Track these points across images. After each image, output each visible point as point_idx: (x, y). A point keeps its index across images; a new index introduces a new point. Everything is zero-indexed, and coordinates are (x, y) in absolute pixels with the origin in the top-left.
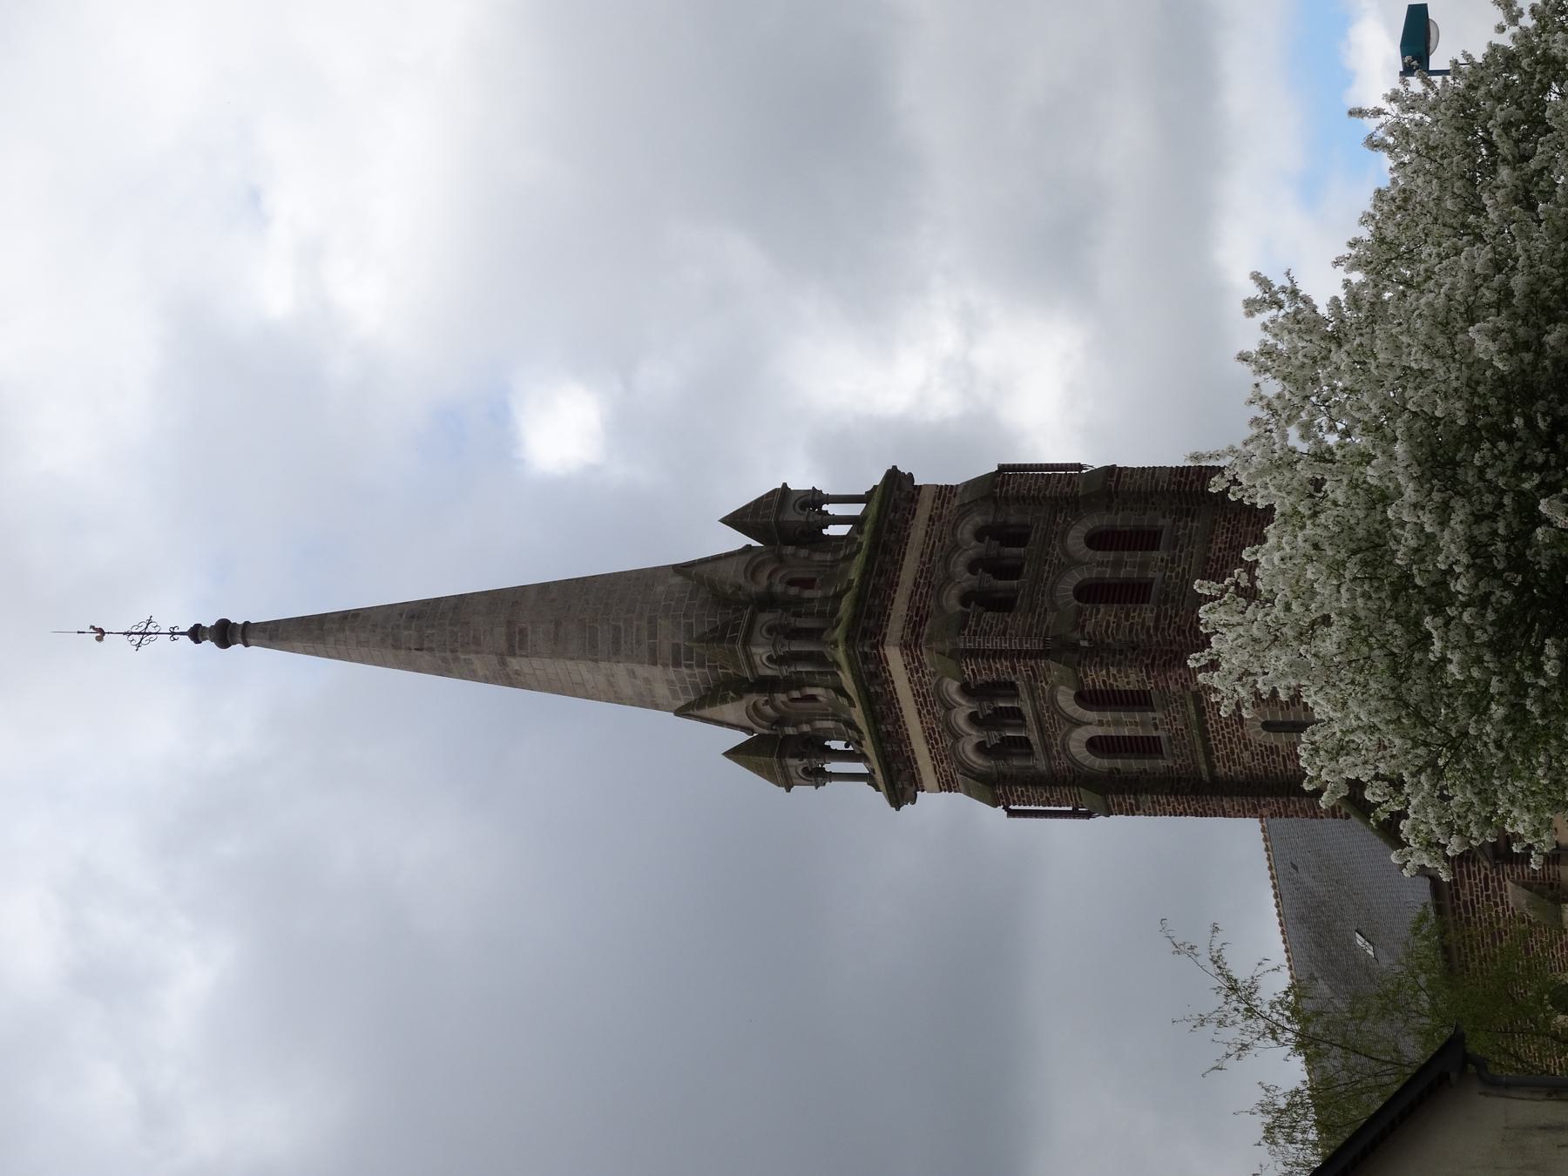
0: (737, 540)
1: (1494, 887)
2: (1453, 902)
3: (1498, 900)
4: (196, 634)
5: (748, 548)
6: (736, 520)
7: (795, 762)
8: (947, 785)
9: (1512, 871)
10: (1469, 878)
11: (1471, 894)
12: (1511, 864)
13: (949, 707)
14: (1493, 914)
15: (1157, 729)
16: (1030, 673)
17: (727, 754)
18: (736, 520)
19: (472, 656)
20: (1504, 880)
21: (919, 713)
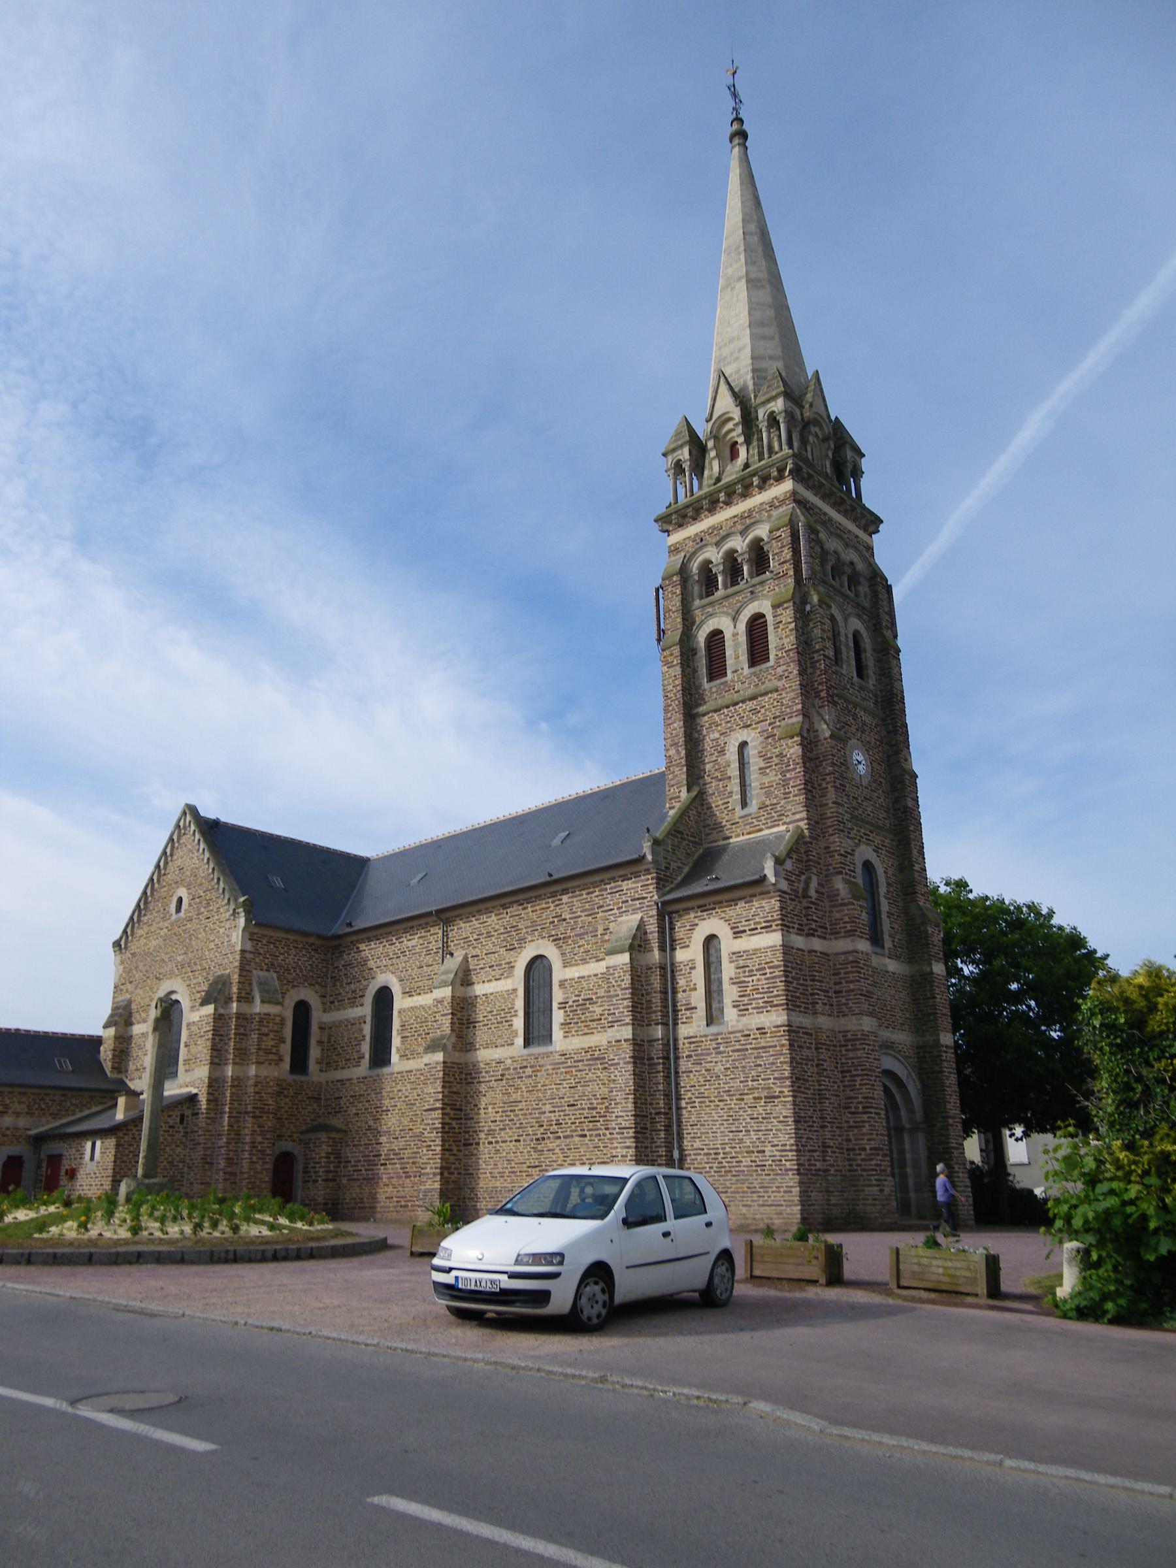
0: (833, 418)
2: (620, 876)
6: (837, 418)
7: (687, 456)
9: (651, 917)
13: (743, 533)
15: (733, 672)
18: (837, 418)
19: (743, 260)
21: (735, 517)
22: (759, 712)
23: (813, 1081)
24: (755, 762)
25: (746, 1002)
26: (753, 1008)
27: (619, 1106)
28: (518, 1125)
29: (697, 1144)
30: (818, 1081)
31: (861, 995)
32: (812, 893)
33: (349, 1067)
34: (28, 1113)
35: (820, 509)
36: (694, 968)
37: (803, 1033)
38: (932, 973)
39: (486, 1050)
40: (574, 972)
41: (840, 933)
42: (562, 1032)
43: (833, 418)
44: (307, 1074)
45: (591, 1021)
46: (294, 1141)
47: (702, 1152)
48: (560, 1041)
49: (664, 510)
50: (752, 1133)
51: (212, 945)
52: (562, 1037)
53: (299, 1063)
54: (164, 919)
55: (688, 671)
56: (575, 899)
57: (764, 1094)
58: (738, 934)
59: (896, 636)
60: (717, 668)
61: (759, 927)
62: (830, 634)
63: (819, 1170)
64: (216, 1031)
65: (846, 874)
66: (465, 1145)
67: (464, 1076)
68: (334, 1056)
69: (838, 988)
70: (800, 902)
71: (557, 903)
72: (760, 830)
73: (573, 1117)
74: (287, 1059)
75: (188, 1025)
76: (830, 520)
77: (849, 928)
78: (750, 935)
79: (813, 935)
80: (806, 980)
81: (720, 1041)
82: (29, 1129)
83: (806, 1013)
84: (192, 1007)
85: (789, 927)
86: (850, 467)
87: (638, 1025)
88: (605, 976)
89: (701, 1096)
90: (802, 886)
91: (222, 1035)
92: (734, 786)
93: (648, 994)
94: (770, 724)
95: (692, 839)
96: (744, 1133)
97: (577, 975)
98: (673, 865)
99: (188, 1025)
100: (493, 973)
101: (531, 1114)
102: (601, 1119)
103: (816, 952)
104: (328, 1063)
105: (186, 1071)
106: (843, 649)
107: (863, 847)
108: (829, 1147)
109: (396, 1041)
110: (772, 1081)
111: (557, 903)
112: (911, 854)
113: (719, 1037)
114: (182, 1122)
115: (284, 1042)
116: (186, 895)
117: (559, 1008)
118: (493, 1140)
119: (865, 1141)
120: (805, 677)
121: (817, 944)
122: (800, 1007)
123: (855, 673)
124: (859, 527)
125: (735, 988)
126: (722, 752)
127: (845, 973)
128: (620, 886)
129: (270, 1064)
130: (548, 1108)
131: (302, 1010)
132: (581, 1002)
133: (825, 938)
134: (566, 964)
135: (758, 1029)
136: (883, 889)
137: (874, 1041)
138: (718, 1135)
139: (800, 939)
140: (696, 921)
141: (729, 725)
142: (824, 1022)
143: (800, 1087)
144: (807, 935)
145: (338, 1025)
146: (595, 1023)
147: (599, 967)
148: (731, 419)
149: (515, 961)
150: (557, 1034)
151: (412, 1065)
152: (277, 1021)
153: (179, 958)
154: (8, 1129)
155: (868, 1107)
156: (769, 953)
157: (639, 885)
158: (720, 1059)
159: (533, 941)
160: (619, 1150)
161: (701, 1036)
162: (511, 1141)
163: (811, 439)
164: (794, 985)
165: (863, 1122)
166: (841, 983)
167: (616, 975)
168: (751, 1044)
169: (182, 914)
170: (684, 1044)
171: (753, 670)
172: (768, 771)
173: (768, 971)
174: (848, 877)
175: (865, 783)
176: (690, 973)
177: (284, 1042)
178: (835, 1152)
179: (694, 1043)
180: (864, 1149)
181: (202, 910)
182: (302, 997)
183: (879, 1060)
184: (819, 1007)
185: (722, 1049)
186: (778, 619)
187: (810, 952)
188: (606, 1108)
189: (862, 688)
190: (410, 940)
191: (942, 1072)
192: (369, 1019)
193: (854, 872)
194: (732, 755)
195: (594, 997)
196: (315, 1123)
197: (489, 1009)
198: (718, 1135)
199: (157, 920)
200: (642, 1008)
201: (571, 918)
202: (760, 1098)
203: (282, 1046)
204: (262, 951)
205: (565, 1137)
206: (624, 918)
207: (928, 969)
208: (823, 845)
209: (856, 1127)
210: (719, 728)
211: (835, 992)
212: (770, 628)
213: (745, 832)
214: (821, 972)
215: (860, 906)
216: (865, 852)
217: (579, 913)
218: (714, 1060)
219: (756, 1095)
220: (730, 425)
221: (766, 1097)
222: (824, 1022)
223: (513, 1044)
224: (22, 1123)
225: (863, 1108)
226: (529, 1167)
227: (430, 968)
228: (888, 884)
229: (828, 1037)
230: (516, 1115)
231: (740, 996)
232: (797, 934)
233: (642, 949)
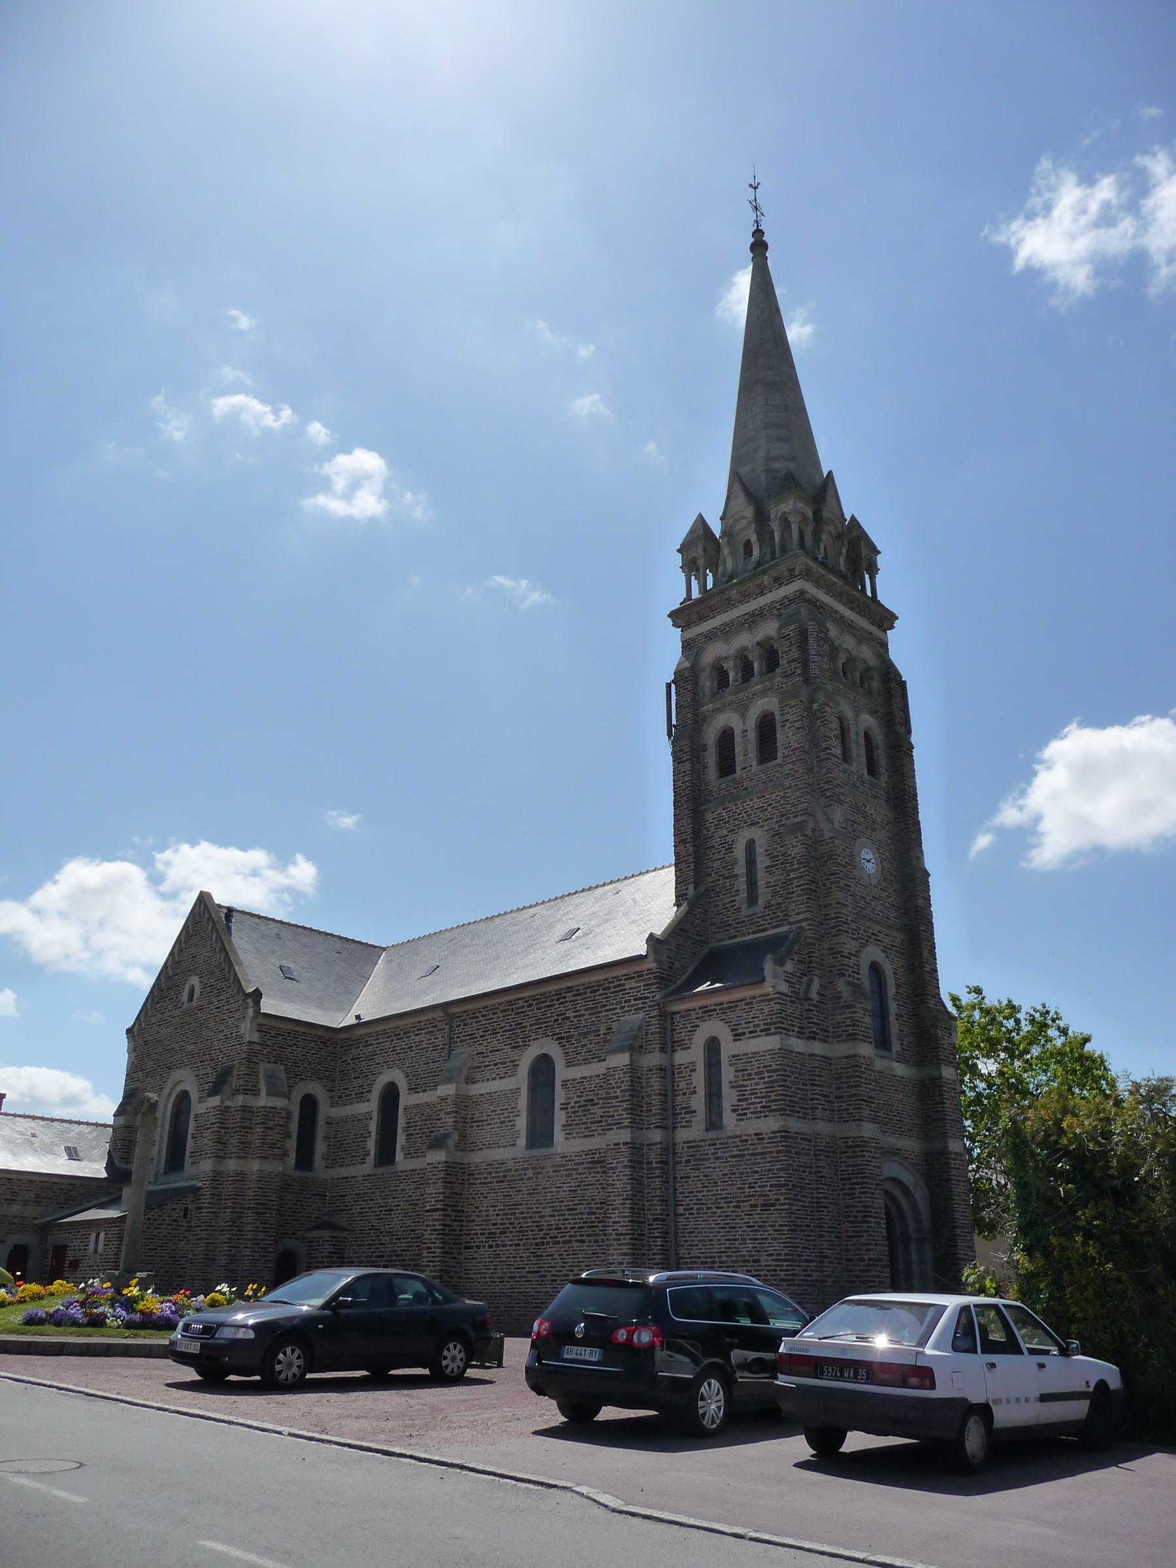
0: (848, 517)
1: (638, 1004)
3: (626, 1009)
4: (758, 233)
5: (846, 520)
7: (701, 551)
8: (687, 645)
10: (644, 986)
11: (630, 989)
12: (659, 1016)
14: (614, 1006)
15: (743, 769)
16: (789, 672)
17: (700, 514)
20: (644, 1012)
21: (745, 614)
22: (767, 809)
23: (811, 1189)
24: (762, 861)
25: (745, 1106)
26: (751, 1113)
27: (617, 1212)
28: (518, 1229)
29: (694, 1252)
30: (817, 1189)
31: (862, 1100)
32: (814, 995)
33: (354, 1164)
34: (35, 1201)
35: (832, 608)
36: (694, 1070)
37: (802, 1139)
38: (940, 1078)
39: (489, 1151)
40: (577, 1073)
41: (842, 1036)
42: (563, 1134)
43: (848, 517)
44: (310, 1170)
45: (591, 1123)
46: (298, 1239)
47: (699, 1261)
48: (562, 1143)
49: (679, 606)
50: (748, 1241)
51: (221, 1036)
52: (563, 1140)
53: (305, 1158)
54: (176, 1007)
55: (698, 766)
56: (579, 998)
57: (761, 1201)
58: (737, 1036)
59: (909, 732)
60: (727, 765)
61: (758, 1029)
62: (838, 732)
63: (816, 1281)
64: (222, 1123)
65: (850, 976)
66: (467, 1248)
67: (466, 1177)
68: (340, 1154)
69: (839, 1093)
70: (802, 1004)
71: (562, 1000)
72: (766, 930)
73: (572, 1222)
74: (293, 1154)
75: (196, 1116)
76: (842, 617)
77: (851, 1031)
78: (750, 1038)
79: (814, 1038)
80: (805, 1085)
81: (718, 1146)
82: (36, 1218)
83: (805, 1118)
84: (200, 1098)
85: (788, 1030)
86: (864, 563)
87: (637, 1128)
88: (606, 1077)
89: (699, 1202)
90: (803, 988)
91: (228, 1128)
92: (741, 885)
93: (648, 1096)
94: (777, 822)
95: (699, 938)
96: (740, 1241)
97: (579, 1075)
98: (677, 964)
99: (196, 1116)
100: (497, 1071)
101: (531, 1217)
102: (600, 1225)
103: (817, 1055)
104: (333, 1160)
105: (192, 1163)
106: (853, 746)
107: (870, 948)
108: (826, 1257)
109: (401, 1139)
110: (768, 1188)
111: (562, 1000)
112: (921, 954)
113: (718, 1142)
114: (185, 1216)
115: (290, 1137)
116: (198, 984)
117: (562, 1109)
118: (494, 1244)
119: (864, 1252)
120: (811, 775)
121: (817, 1048)
122: (799, 1112)
123: (866, 770)
124: (873, 624)
125: (734, 1092)
126: (730, 849)
127: (848, 1077)
128: (624, 985)
129: (275, 1159)
130: (548, 1211)
131: (309, 1104)
132: (583, 1103)
133: (826, 1042)
134: (569, 1064)
135: (756, 1134)
136: (891, 991)
137: (875, 1148)
138: (715, 1243)
139: (800, 1042)
140: (698, 1022)
141: (737, 822)
142: (822, 1127)
143: (796, 1195)
144: (809, 1038)
145: (344, 1120)
146: (596, 1125)
147: (597, 1068)
148: (743, 518)
149: (520, 1059)
150: (559, 1135)
151: (415, 1164)
152: (283, 1115)
153: (190, 1048)
154: (15, 1217)
155: (867, 1216)
156: (768, 1057)
157: (642, 984)
158: (718, 1164)
159: (538, 1039)
160: (615, 1257)
161: (700, 1141)
162: (511, 1245)
163: (824, 537)
164: (793, 1089)
165: (861, 1231)
166: (842, 1088)
167: (617, 1076)
168: (749, 1149)
169: (194, 1003)
170: (683, 1148)
171: (761, 767)
172: (774, 869)
173: (766, 1075)
174: (851, 979)
175: (874, 882)
176: (690, 1076)
177: (290, 1137)
178: (833, 1263)
179: (693, 1147)
180: (863, 1260)
181: (214, 999)
182: (310, 1091)
183: (880, 1168)
184: (819, 1112)
185: (720, 1154)
186: (786, 717)
187: (810, 1055)
188: (605, 1213)
189: (873, 786)
190: (416, 1035)
191: (951, 1179)
192: (375, 1115)
193: (858, 974)
194: (739, 852)
195: (595, 1098)
196: (319, 1220)
197: (492, 1108)
198: (715, 1243)
199: (170, 1007)
200: (642, 1111)
201: (574, 1017)
202: (756, 1206)
203: (288, 1140)
204: (269, 1043)
205: (565, 1242)
206: (627, 1018)
207: (937, 1073)
208: (827, 946)
209: (856, 1237)
210: (727, 825)
211: (836, 1097)
212: (778, 726)
213: (751, 931)
214: (821, 1076)
215: (863, 1009)
216: (873, 953)
217: (583, 1012)
218: (713, 1165)
219: (753, 1202)
220: (743, 524)
221: (763, 1205)
222: (822, 1127)
223: (515, 1145)
224: (29, 1211)
225: (862, 1217)
226: (528, 1272)
227: (437, 1065)
228: (898, 986)
229: (827, 1143)
230: (517, 1219)
231: (739, 1100)
232: (797, 1037)
233: (644, 1050)
